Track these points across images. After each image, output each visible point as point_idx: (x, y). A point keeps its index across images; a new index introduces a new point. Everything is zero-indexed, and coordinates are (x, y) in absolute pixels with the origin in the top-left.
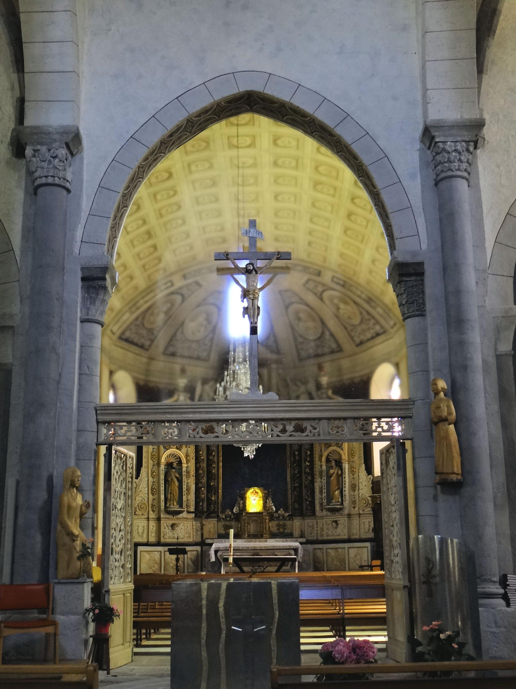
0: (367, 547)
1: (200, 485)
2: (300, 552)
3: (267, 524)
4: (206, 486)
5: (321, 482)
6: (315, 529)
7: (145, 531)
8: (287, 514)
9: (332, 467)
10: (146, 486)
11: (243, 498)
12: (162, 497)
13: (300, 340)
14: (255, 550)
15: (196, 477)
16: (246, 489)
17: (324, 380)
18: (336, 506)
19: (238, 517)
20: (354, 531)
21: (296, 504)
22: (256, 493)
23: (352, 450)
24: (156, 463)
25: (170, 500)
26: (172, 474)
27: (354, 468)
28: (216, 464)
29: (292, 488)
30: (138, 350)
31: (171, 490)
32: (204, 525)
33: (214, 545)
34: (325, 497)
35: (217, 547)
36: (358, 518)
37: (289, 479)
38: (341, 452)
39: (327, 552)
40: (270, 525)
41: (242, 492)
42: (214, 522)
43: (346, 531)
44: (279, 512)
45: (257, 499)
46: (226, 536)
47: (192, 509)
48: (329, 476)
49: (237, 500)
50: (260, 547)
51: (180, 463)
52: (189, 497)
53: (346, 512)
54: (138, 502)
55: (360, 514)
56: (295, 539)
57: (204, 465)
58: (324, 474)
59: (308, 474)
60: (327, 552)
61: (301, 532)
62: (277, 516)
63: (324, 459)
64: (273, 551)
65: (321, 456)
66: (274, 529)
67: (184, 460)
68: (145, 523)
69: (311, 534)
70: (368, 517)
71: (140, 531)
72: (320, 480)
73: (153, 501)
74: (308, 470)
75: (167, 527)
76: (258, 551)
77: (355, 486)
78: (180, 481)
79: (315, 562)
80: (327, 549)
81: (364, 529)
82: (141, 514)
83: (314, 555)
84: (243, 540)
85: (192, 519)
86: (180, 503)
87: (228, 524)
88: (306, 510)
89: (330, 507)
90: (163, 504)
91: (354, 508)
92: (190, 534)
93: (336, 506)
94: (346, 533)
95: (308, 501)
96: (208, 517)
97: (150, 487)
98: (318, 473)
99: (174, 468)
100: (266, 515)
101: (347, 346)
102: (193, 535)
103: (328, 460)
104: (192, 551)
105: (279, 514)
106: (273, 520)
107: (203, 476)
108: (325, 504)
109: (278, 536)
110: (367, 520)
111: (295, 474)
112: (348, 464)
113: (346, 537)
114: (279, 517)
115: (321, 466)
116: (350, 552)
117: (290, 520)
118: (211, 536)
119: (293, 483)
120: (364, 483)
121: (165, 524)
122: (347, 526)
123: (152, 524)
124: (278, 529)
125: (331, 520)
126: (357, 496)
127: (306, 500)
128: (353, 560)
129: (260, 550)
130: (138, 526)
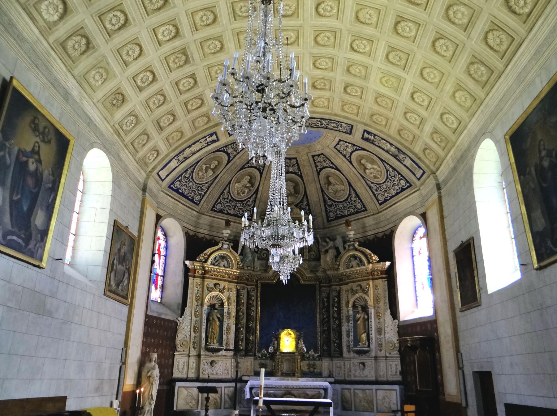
0: (396, 390)
1: (240, 326)
2: (330, 392)
3: (299, 364)
4: (245, 327)
5: (348, 326)
6: (343, 369)
7: (185, 367)
8: (316, 355)
9: (358, 312)
10: (189, 324)
11: (278, 339)
12: (204, 335)
13: (330, 203)
14: (287, 388)
15: (236, 318)
16: (280, 330)
17: (351, 234)
18: (364, 349)
19: (272, 356)
20: (382, 373)
21: (325, 345)
22: (290, 334)
23: (378, 297)
24: (199, 303)
25: (211, 338)
26: (214, 314)
27: (379, 312)
28: (255, 307)
29: (322, 331)
30: (189, 203)
31: (212, 328)
32: (239, 363)
33: (249, 382)
34: (352, 340)
35: (252, 384)
36: (384, 361)
37: (318, 324)
38: (367, 298)
39: (354, 393)
40: (302, 365)
41: (277, 333)
42: (251, 360)
43: (373, 373)
44: (310, 353)
45: (290, 340)
46: (257, 374)
47: (232, 347)
48: (356, 321)
49: (272, 341)
50: (292, 386)
51: (222, 304)
52: (229, 336)
53: (373, 354)
54: (180, 339)
55: (386, 357)
56: (325, 379)
57: (244, 308)
58: (351, 318)
59: (336, 318)
60: (354, 393)
61: (330, 372)
62: (308, 356)
63: (351, 305)
64: (305, 390)
65: (348, 302)
66: (305, 369)
67: (226, 303)
68: (185, 359)
69: (339, 374)
70: (394, 360)
71: (181, 367)
72: (346, 324)
73: (195, 339)
74: (335, 315)
75: (206, 363)
76: (290, 390)
77: (381, 330)
78: (221, 321)
79: (343, 401)
80: (354, 389)
81: (391, 371)
82: (182, 351)
83: (342, 395)
84: (276, 378)
85: (231, 356)
86: (220, 342)
87: (263, 362)
88: (334, 351)
89: (358, 349)
90: (203, 341)
91: (381, 350)
92: (228, 371)
93: (364, 349)
94: (374, 376)
95: (336, 343)
96: (246, 355)
97: (193, 325)
98: (345, 318)
99: (216, 309)
100: (297, 355)
101: (371, 204)
102: (231, 372)
103: (354, 306)
104: (226, 389)
105: (309, 355)
106: (304, 360)
107: (243, 318)
108: (352, 346)
109: (309, 375)
110: (394, 363)
111: (324, 319)
112: (374, 309)
113: (373, 379)
114: (309, 357)
115: (348, 311)
116: (378, 394)
117: (319, 360)
118: (248, 373)
119: (322, 326)
120: (390, 327)
121: (204, 361)
122: (374, 367)
123: (192, 360)
124: (309, 369)
125: (358, 361)
126: (383, 339)
127: (334, 342)
128: (381, 403)
129: (292, 388)
130: (179, 362)
